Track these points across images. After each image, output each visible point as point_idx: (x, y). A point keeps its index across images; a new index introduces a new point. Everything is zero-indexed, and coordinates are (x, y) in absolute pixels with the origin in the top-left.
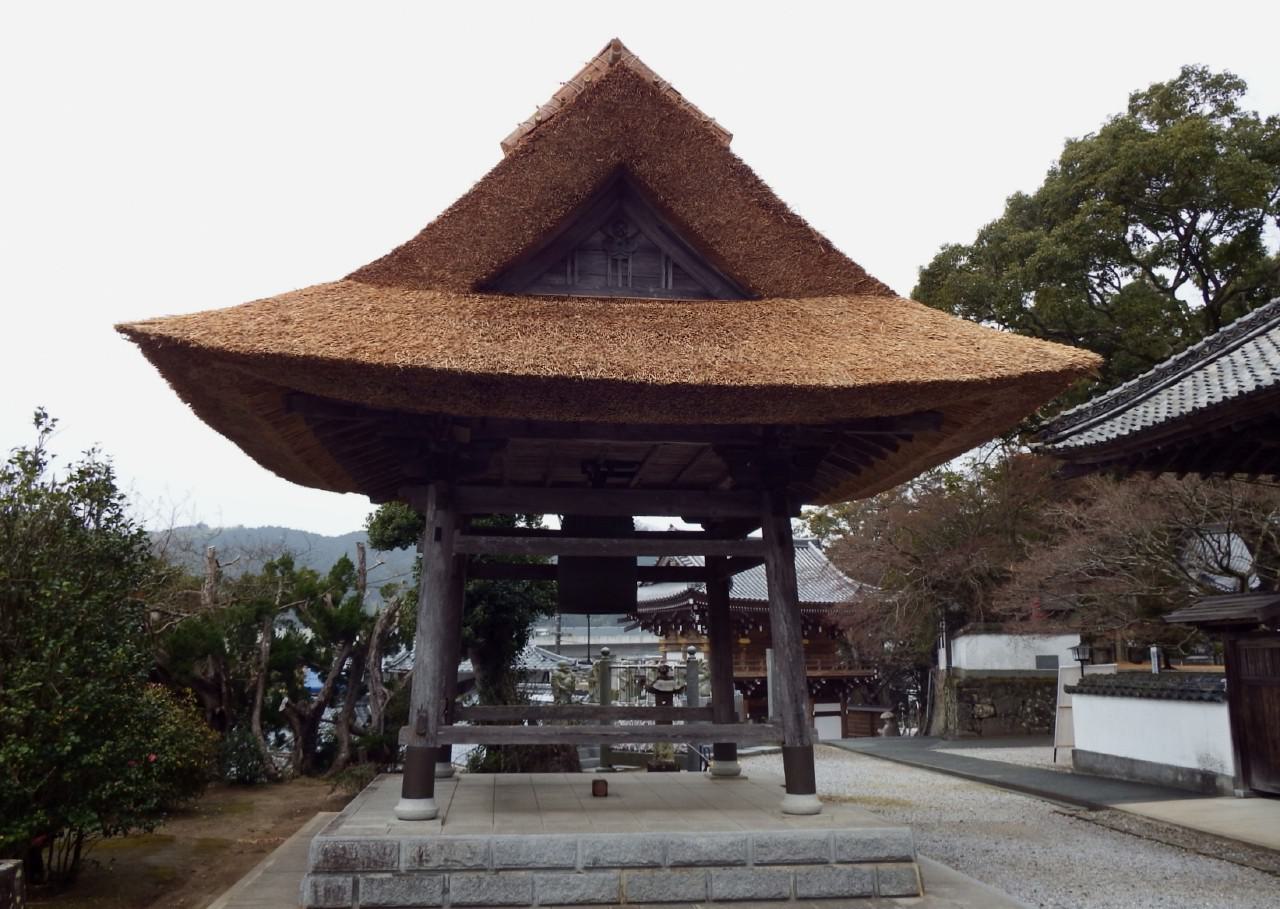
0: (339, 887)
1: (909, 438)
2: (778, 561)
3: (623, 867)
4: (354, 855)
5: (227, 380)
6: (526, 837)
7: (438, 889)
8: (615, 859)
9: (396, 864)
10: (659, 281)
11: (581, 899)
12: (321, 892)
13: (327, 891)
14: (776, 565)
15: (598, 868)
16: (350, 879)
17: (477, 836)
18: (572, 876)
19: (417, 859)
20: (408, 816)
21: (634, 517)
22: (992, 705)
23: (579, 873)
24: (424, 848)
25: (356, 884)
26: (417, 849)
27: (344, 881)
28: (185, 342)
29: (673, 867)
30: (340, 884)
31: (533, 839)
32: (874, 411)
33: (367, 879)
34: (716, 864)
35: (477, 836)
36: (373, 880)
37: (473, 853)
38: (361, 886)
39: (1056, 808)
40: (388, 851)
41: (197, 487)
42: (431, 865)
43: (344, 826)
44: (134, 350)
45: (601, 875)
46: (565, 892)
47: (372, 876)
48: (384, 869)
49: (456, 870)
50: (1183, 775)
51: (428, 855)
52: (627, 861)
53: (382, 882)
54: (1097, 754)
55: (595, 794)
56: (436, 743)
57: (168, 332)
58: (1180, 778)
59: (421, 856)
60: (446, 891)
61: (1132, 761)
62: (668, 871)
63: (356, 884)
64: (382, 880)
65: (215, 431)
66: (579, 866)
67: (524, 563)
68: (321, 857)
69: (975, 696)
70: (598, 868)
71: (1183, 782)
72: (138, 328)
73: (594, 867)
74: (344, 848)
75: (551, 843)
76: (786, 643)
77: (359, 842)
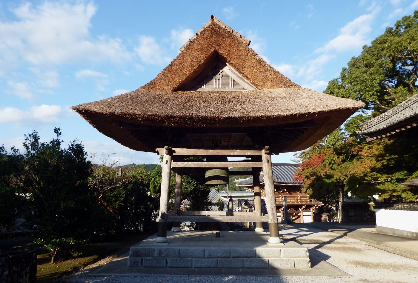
0: (138, 261)
1: (306, 129)
2: (267, 168)
3: (218, 257)
4: (141, 252)
5: (103, 120)
6: (190, 248)
7: (165, 262)
8: (216, 255)
9: (153, 255)
10: (229, 86)
11: (206, 266)
12: (133, 262)
13: (134, 262)
14: (266, 169)
15: (211, 257)
16: (140, 259)
17: (176, 248)
18: (203, 260)
19: (159, 254)
20: (158, 242)
21: (228, 157)
22: (355, 212)
23: (205, 259)
24: (161, 251)
25: (142, 260)
26: (159, 251)
27: (138, 259)
28: (181, 116)
29: (233, 257)
30: (138, 260)
31: (192, 248)
32: (292, 122)
33: (145, 259)
34: (246, 257)
35: (176, 248)
36: (147, 259)
37: (175, 252)
38: (143, 261)
39: (366, 243)
40: (151, 251)
41: (107, 153)
42: (163, 255)
43: (141, 244)
44: (77, 114)
45: (211, 259)
46: (201, 264)
47: (147, 258)
48: (150, 256)
49: (170, 257)
50: (410, 234)
51: (162, 253)
52: (219, 255)
53: (149, 260)
54: (383, 227)
55: (216, 237)
56: (167, 221)
57: (117, 110)
58: (409, 235)
59: (160, 253)
60: (167, 263)
61: (394, 229)
62: (232, 259)
63: (142, 260)
64: (149, 259)
65: (106, 136)
66: (206, 257)
67: (18, 154)
68: (132, 252)
69: (349, 210)
70: (211, 257)
71: (410, 236)
72: (95, 109)
73: (210, 257)
74: (139, 250)
75: (197, 250)
76: (269, 192)
77: (143, 248)
